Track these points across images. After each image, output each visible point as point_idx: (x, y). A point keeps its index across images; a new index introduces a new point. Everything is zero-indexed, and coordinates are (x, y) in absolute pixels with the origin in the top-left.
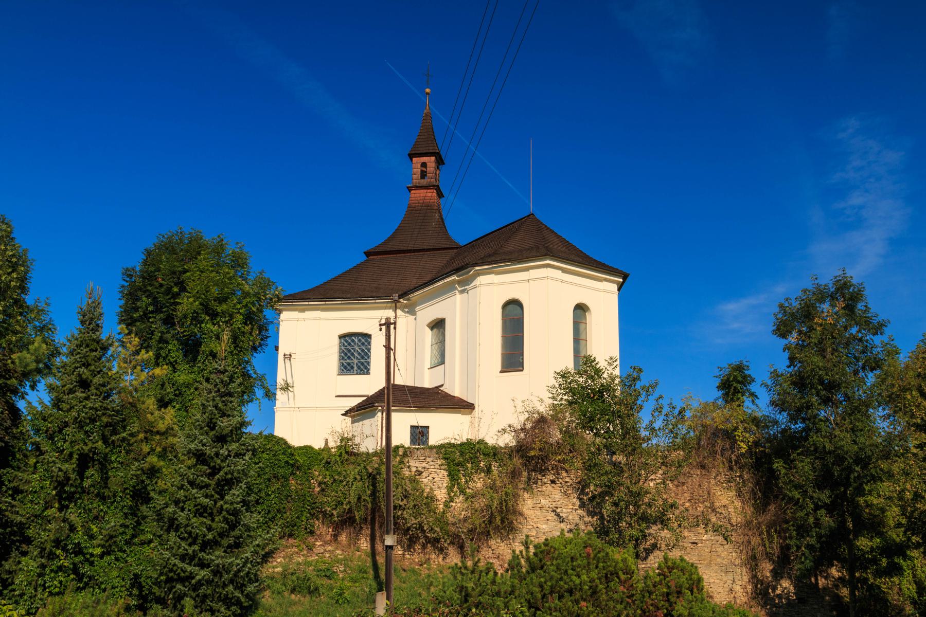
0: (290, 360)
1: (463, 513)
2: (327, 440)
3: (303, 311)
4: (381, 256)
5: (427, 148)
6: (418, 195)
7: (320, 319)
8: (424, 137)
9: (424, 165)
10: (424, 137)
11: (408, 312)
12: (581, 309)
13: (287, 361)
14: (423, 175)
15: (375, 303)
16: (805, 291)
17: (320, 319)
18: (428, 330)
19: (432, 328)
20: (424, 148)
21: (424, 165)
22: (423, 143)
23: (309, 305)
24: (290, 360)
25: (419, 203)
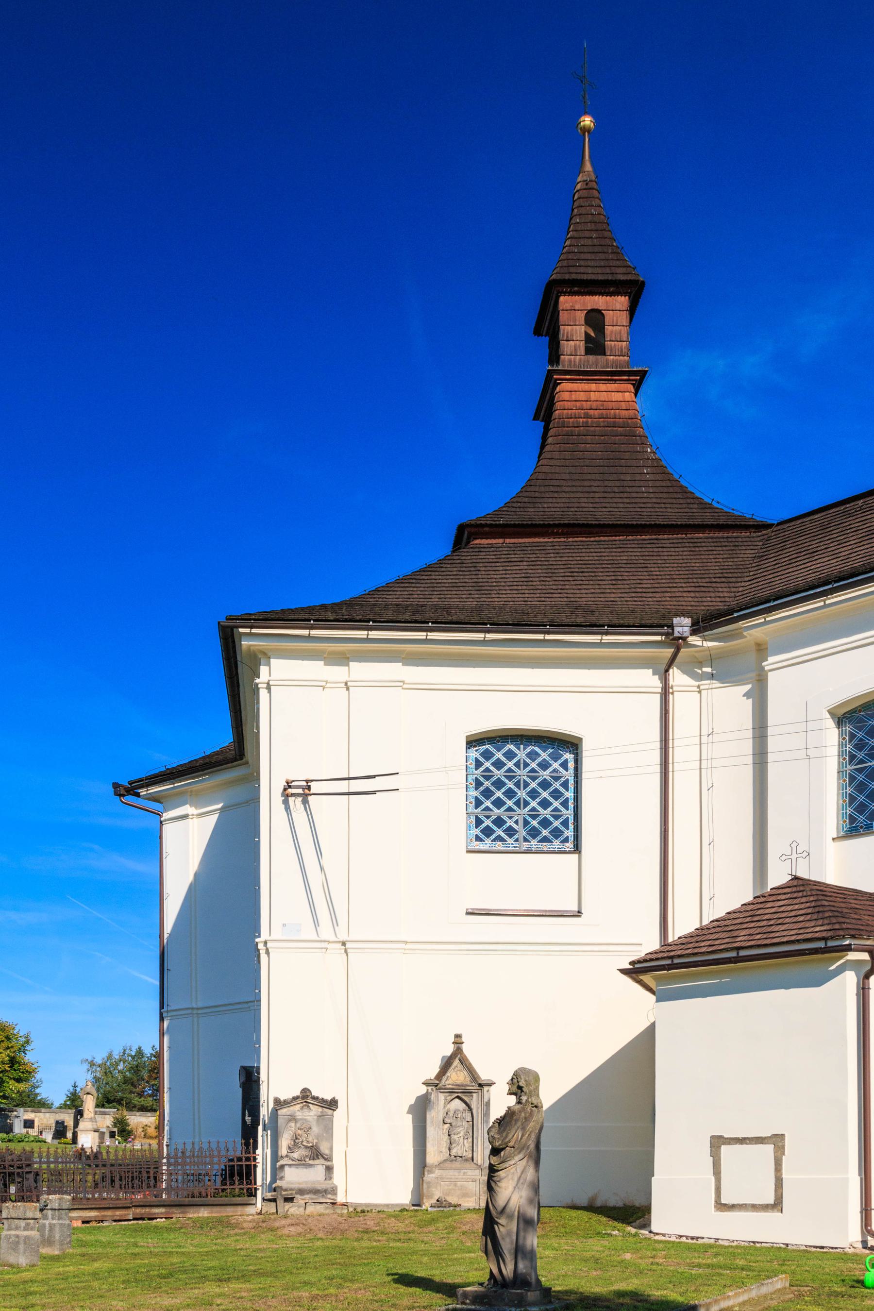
0: (305, 802)
1: (731, 1294)
2: (458, 1036)
3: (342, 659)
4: (513, 541)
5: (608, 270)
6: (582, 396)
7: (401, 684)
8: (589, 242)
9: (595, 319)
10: (589, 242)
11: (712, 676)
12: (270, 935)
13: (296, 804)
14: (595, 346)
15: (600, 645)
16: (61, 1104)
17: (401, 684)
18: (830, 723)
19: (840, 722)
20: (599, 270)
21: (595, 319)
22: (588, 256)
23: (367, 640)
24: (305, 802)
25: (587, 416)
